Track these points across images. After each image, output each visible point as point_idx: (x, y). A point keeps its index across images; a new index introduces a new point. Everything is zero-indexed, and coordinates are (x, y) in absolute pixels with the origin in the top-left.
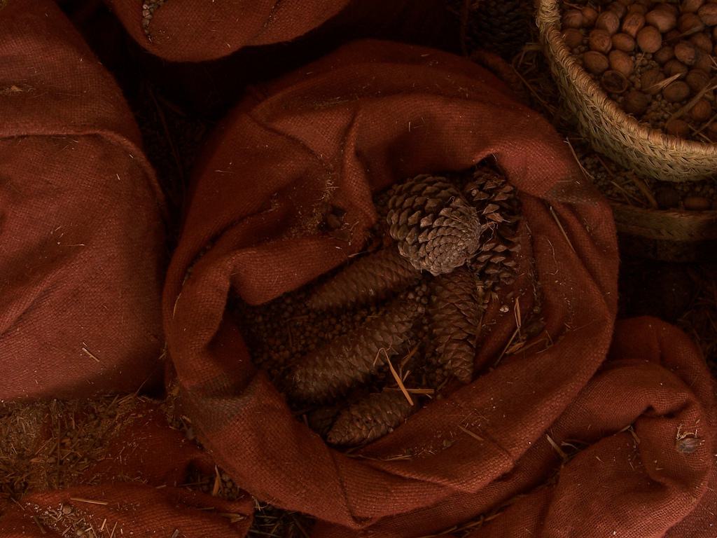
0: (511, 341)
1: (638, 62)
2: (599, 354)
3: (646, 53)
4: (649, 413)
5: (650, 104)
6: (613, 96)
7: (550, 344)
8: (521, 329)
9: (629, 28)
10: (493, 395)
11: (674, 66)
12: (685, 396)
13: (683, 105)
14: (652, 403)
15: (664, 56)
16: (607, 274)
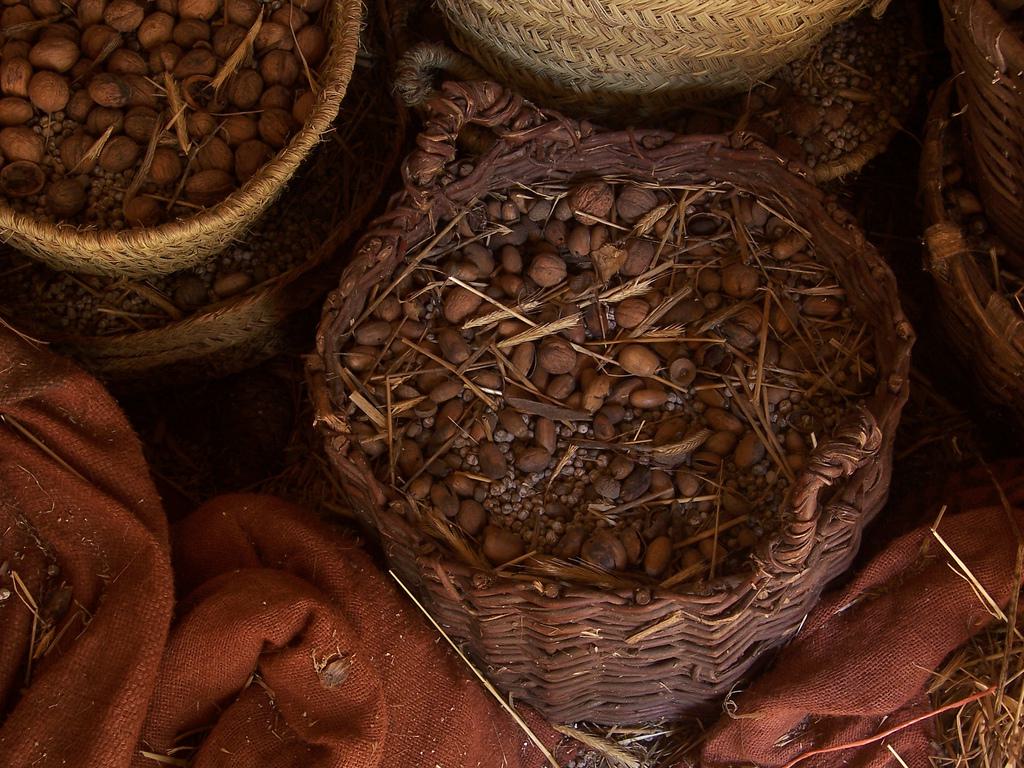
0: (33, 639)
1: (47, 132)
2: (164, 601)
3: (54, 113)
4: (269, 653)
5: (89, 188)
6: (31, 200)
7: (88, 618)
8: (41, 614)
9: (12, 85)
10: (36, 737)
11: (99, 119)
12: (303, 606)
13: (137, 169)
14: (264, 635)
15: (80, 109)
16: (127, 475)
